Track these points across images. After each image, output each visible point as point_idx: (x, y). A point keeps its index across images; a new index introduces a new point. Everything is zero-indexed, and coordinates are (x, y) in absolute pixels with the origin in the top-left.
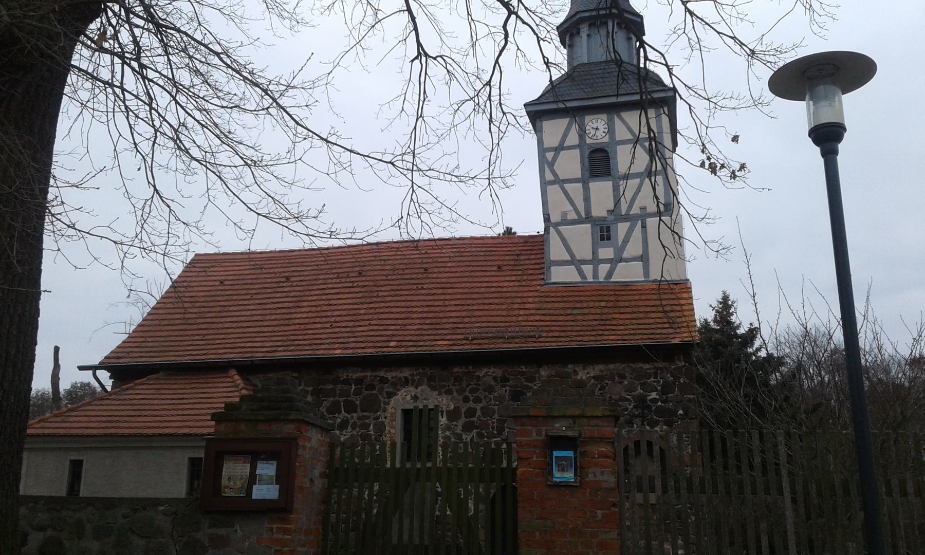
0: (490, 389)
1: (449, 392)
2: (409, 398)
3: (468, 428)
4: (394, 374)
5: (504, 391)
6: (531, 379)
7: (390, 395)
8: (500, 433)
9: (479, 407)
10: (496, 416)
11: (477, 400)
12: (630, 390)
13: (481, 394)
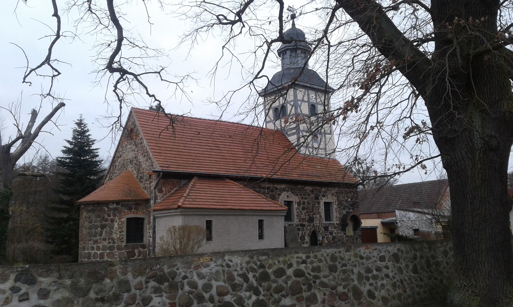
0: (309, 195)
1: (297, 195)
2: (286, 196)
3: (303, 209)
4: (280, 186)
5: (313, 196)
6: (320, 192)
7: (279, 195)
8: (312, 211)
9: (306, 201)
10: (311, 205)
11: (306, 199)
12: (344, 198)
13: (307, 196)
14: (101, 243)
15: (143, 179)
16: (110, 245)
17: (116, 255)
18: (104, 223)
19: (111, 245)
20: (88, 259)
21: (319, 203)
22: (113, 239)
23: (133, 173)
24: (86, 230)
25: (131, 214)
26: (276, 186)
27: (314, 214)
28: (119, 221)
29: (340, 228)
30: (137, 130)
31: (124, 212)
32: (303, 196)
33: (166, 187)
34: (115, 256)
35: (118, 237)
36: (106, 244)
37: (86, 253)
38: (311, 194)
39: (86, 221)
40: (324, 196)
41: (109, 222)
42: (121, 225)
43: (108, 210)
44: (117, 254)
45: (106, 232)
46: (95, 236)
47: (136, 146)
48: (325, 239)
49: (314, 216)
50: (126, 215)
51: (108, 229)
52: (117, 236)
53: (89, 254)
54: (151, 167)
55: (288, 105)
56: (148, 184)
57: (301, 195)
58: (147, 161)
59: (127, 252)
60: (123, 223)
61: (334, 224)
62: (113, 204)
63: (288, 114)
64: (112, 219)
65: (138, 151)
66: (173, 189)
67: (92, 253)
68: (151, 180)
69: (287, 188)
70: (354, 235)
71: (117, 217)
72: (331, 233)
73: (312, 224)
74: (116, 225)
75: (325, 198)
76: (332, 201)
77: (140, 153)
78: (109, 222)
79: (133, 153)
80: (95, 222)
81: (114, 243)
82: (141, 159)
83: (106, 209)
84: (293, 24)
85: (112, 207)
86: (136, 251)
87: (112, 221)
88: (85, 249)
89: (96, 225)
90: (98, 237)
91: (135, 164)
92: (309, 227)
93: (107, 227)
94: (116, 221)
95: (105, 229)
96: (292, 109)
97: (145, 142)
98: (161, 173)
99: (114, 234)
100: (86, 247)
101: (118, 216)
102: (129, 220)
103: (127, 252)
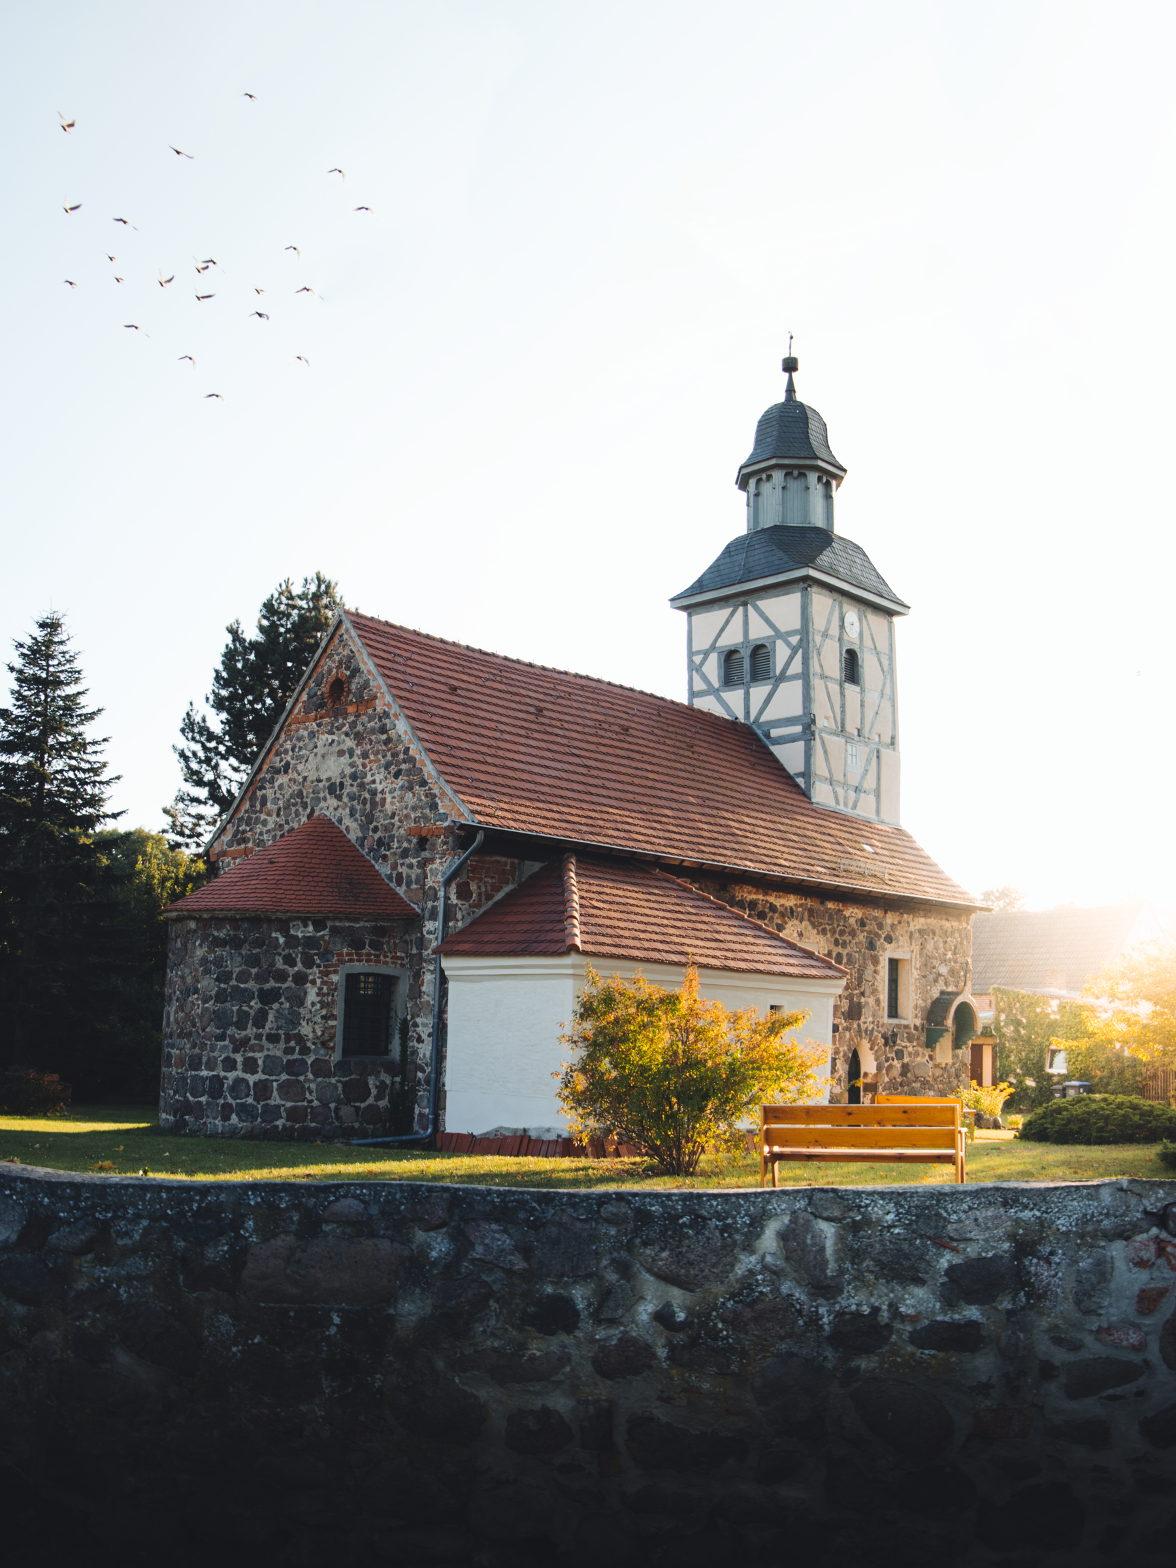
1: (824, 932)
5: (861, 937)
8: (859, 985)
9: (844, 952)
10: (857, 966)
11: (844, 945)
13: (847, 938)
14: (261, 1048)
15: (389, 848)
16: (290, 1057)
17: (311, 1092)
18: (272, 984)
19: (296, 1056)
20: (212, 1096)
21: (875, 961)
22: (300, 1039)
23: (343, 828)
24: (205, 1002)
25: (360, 961)
26: (772, 899)
27: (863, 994)
28: (323, 983)
29: (923, 1039)
30: (366, 685)
31: (338, 955)
32: (837, 936)
33: (480, 880)
34: (307, 1095)
35: (319, 1033)
36: (279, 1053)
37: (203, 1079)
38: (858, 932)
39: (207, 971)
40: (889, 939)
41: (289, 983)
42: (328, 994)
43: (286, 943)
44: (313, 1086)
45: (279, 1015)
46: (241, 1026)
47: (359, 738)
48: (884, 1071)
49: (863, 1000)
50: (342, 962)
51: (287, 1005)
52: (314, 1031)
53: (218, 1081)
54: (427, 811)
55: (780, 644)
56: (411, 866)
57: (833, 932)
58: (410, 788)
59: (345, 1084)
60: (335, 989)
61: (906, 1027)
62: (306, 926)
63: (778, 672)
64: (298, 972)
65: (365, 755)
66: (501, 888)
67: (226, 1078)
68: (426, 854)
69: (800, 909)
70: (954, 1064)
71: (315, 969)
72: (900, 1055)
73: (855, 1026)
74: (312, 996)
75: (893, 945)
76: (907, 956)
77: (377, 761)
78: (289, 983)
79: (345, 760)
80: (243, 977)
81: (305, 1051)
82: (379, 780)
83: (282, 940)
84: (790, 390)
85: (300, 935)
86: (372, 1082)
87: (301, 979)
88: (200, 1063)
89: (246, 990)
90: (251, 1031)
91: (352, 797)
92: (848, 1035)
93: (282, 1000)
94: (313, 982)
95: (276, 1006)
96: (791, 658)
97: (402, 727)
98: (480, 837)
99: (304, 1023)
100: (204, 1059)
101: (318, 966)
102: (352, 980)
103: (345, 1084)
